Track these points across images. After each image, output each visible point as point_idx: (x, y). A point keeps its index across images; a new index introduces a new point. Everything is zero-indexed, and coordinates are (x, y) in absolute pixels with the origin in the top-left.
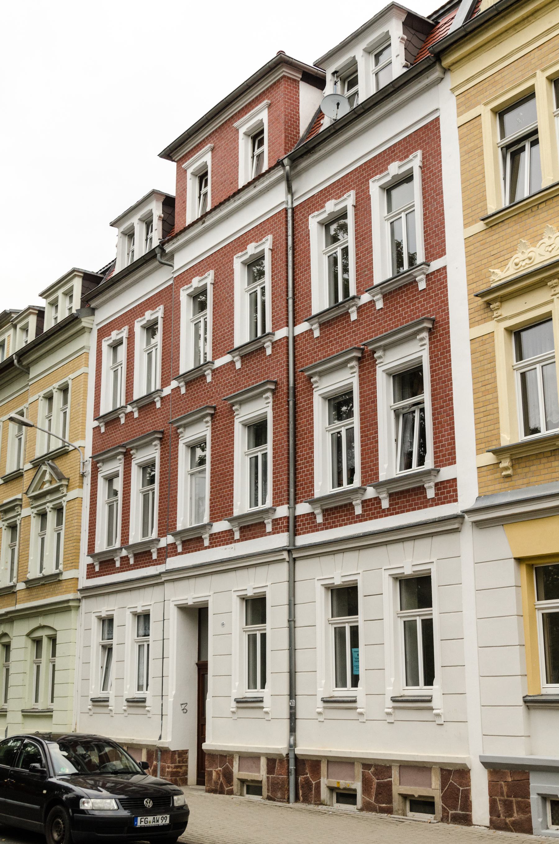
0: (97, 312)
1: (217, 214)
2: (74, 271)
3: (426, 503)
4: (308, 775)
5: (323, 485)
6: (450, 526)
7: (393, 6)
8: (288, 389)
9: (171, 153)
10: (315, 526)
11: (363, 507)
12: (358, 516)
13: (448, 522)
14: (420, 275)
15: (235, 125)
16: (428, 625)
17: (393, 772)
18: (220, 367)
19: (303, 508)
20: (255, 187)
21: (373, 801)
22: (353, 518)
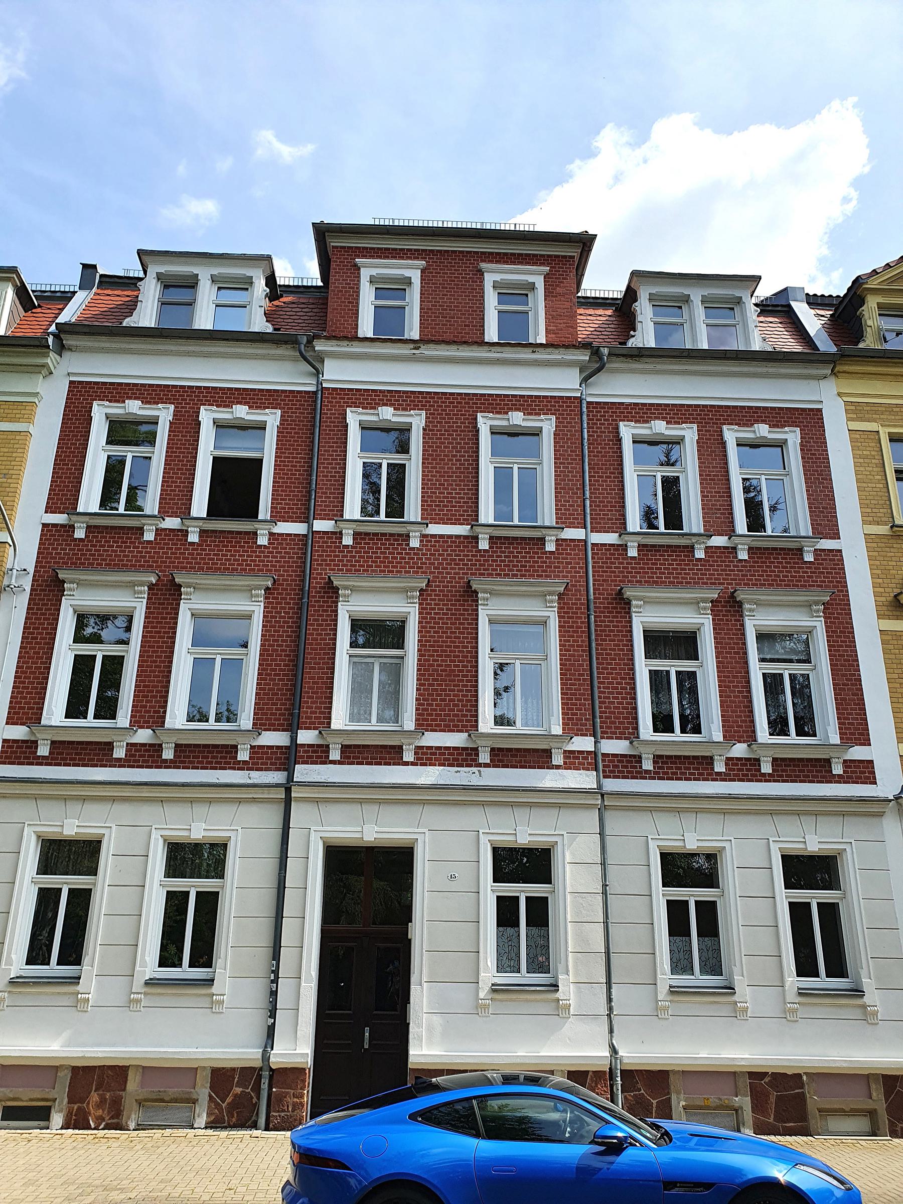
0: (67, 355)
1: (480, 351)
2: (14, 270)
3: (830, 778)
4: (642, 1091)
5: (177, 714)
6: (872, 809)
7: (269, 258)
8: (588, 600)
9: (328, 232)
10: (640, 773)
11: (175, 751)
12: (647, 771)
13: (517, 794)
14: (415, 531)
15: (483, 265)
16: (830, 912)
17: (130, 1074)
18: (433, 536)
19: (306, 737)
20: (533, 352)
21: (771, 1120)
22: (711, 774)
